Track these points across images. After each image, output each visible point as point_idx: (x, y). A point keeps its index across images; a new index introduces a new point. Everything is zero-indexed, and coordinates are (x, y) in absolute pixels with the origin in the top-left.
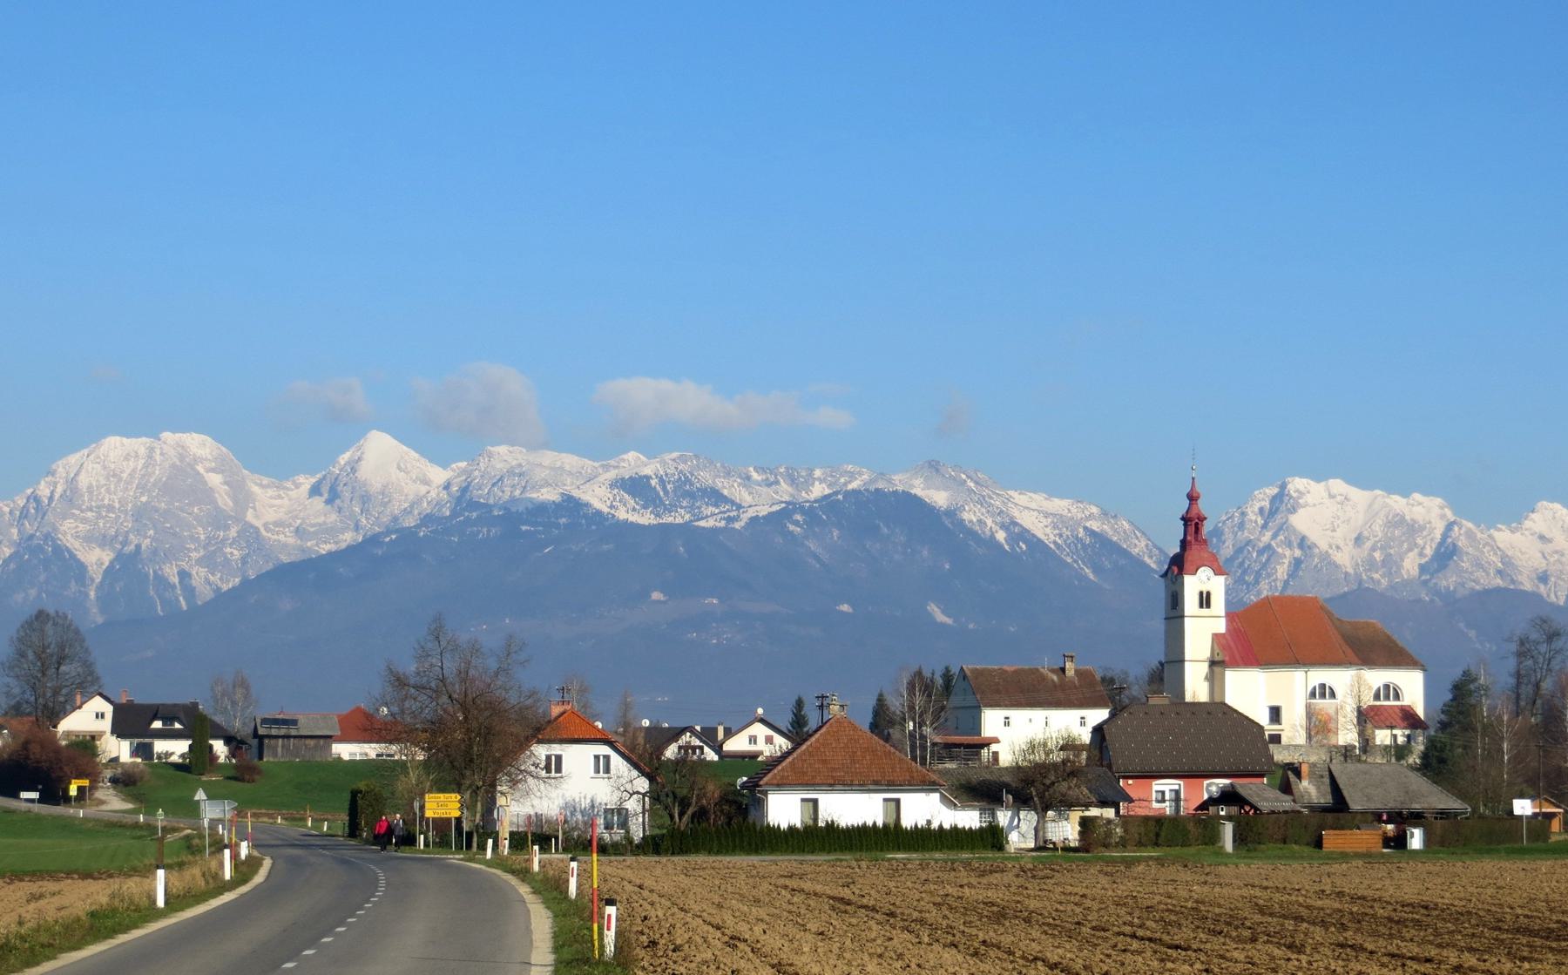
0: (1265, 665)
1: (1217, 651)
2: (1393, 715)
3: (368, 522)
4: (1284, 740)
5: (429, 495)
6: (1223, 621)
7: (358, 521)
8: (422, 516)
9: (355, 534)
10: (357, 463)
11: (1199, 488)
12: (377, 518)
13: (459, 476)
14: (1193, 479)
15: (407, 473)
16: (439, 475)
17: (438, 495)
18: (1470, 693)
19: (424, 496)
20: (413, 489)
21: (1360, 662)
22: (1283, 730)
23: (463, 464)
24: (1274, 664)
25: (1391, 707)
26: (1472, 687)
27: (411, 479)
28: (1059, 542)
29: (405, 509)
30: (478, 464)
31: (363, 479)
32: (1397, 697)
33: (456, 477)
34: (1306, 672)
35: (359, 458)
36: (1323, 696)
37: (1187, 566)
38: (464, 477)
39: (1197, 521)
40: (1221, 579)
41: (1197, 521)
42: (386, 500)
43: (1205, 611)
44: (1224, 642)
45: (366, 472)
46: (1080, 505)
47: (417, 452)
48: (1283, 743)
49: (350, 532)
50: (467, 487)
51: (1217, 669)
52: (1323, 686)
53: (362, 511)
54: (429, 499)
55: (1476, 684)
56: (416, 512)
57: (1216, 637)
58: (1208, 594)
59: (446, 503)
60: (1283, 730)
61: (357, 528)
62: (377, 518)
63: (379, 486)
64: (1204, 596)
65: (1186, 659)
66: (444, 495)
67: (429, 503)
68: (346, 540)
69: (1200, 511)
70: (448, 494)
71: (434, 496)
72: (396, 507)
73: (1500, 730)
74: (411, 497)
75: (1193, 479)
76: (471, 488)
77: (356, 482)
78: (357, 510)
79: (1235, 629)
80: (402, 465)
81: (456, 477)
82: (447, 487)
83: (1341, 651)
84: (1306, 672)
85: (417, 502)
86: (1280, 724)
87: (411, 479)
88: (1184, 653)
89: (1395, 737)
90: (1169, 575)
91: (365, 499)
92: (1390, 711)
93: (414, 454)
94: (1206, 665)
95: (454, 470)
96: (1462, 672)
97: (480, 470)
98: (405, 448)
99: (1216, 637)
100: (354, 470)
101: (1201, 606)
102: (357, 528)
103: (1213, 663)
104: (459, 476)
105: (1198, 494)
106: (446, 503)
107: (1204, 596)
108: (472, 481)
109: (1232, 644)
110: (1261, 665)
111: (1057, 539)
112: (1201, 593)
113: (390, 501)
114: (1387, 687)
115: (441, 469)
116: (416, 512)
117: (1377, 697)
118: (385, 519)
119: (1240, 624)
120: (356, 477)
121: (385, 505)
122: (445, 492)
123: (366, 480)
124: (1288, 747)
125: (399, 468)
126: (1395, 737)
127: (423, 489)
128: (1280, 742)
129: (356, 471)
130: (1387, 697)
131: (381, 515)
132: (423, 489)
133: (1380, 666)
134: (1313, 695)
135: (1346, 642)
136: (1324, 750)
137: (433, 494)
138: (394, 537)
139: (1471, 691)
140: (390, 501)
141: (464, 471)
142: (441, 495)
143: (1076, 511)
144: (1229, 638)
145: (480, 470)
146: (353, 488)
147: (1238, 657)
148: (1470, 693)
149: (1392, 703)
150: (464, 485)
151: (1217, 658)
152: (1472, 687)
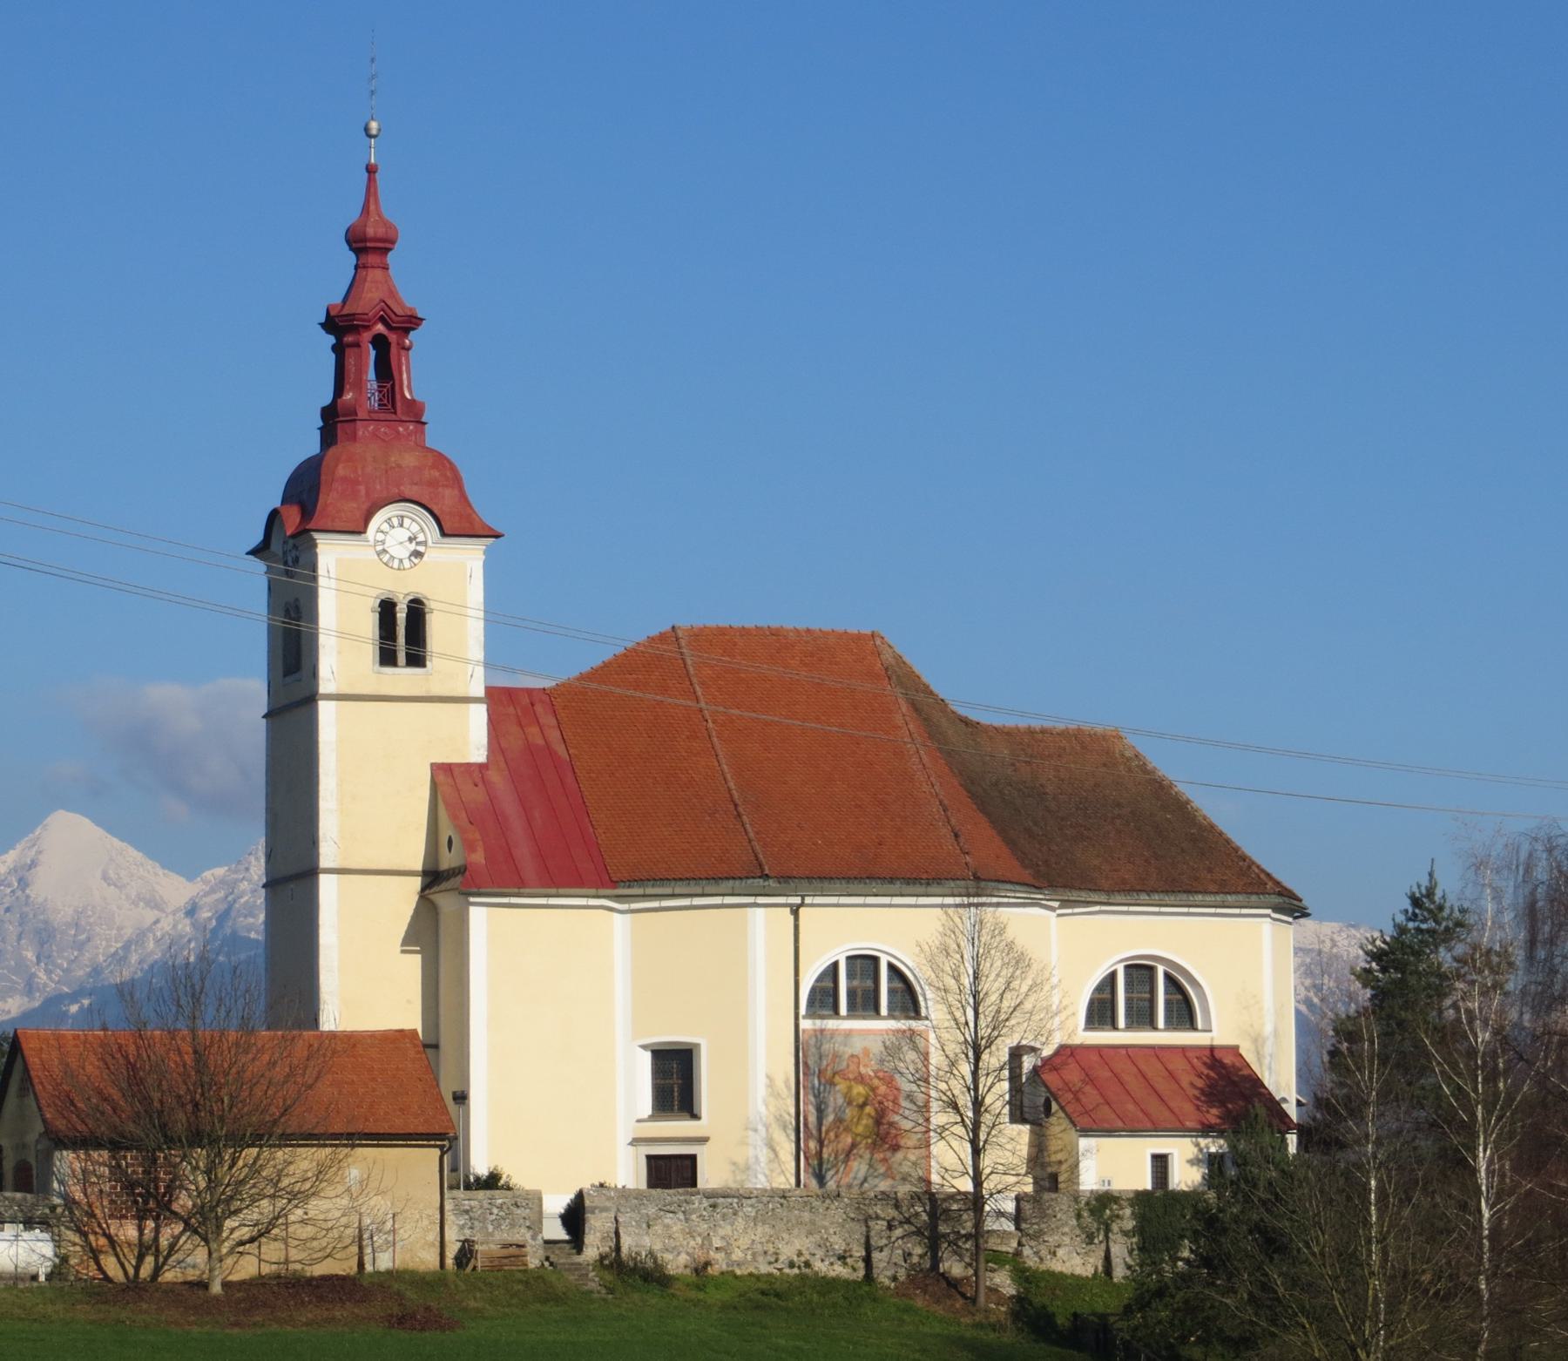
0: (632, 881)
1: (446, 830)
2: (1163, 1086)
3: (51, 979)
4: (710, 1175)
5: (159, 926)
6: (478, 716)
7: (33, 975)
8: (146, 967)
9: (26, 999)
10: (30, 869)
11: (391, 208)
12: (66, 971)
13: (213, 891)
14: (371, 170)
15: (120, 887)
16: (177, 890)
17: (175, 927)
18: (1440, 984)
19: (150, 929)
20: (131, 918)
21: (1026, 874)
22: (703, 1140)
23: (220, 871)
24: (663, 880)
25: (1157, 1052)
26: (1445, 958)
27: (128, 897)
28: (1316, 1000)
29: (116, 953)
30: (247, 869)
31: (40, 900)
32: (1184, 1012)
33: (206, 894)
34: (795, 911)
35: (33, 861)
36: (865, 1003)
37: (329, 499)
38: (221, 894)
39: (380, 328)
40: (470, 557)
41: (380, 328)
42: (83, 937)
43: (402, 678)
44: (476, 796)
45: (44, 888)
46: (1353, 931)
47: (138, 848)
48: (701, 1184)
49: (18, 998)
50: (227, 912)
51: (445, 901)
52: (865, 964)
53: (38, 958)
54: (159, 934)
55: (1460, 949)
56: (134, 958)
57: (444, 775)
58: (417, 611)
59: (189, 941)
60: (703, 1140)
61: (30, 988)
62: (66, 971)
63: (70, 911)
64: (401, 616)
65: (325, 861)
66: (186, 927)
67: (157, 941)
68: (9, 1012)
69: (392, 293)
70: (193, 925)
71: (168, 928)
72: (102, 948)
73: (1459, 1092)
74: (128, 932)
75: (371, 170)
76: (233, 914)
77: (27, 904)
78: (30, 955)
79: (530, 749)
80: (112, 874)
81: (206, 894)
82: (191, 911)
83: (945, 831)
84: (795, 911)
85: (141, 936)
86: (695, 1116)
87: (128, 897)
88: (313, 842)
89: (1161, 1163)
90: (276, 546)
91: (45, 936)
92: (1153, 1070)
93: (134, 854)
94: (417, 883)
95: (205, 882)
96: (1407, 904)
97: (250, 881)
98: (116, 841)
99: (444, 775)
100: (23, 883)
101: (387, 658)
102: (30, 988)
103: (433, 877)
104: (213, 891)
105: (389, 226)
106: (189, 941)
107: (401, 616)
108: (235, 901)
109: (510, 806)
110: (614, 884)
111: (1311, 994)
112: (387, 609)
113: (89, 939)
114: (1140, 972)
115: (182, 879)
116: (134, 958)
117: (1100, 1012)
118: (81, 973)
119: (554, 735)
120: (28, 897)
121: (80, 946)
122: (187, 921)
123: (46, 900)
124: (727, 1200)
125: (105, 878)
126: (1161, 1163)
127: (150, 915)
128: (692, 1181)
129: (27, 885)
130: (1142, 1016)
131: (74, 966)
132: (150, 915)
133: (1109, 892)
134: (823, 998)
135: (982, 805)
136: (837, 1212)
137: (166, 925)
138: (86, 1002)
139: (1443, 977)
140: (89, 939)
141: (222, 882)
142: (180, 927)
143: (1346, 942)
144: (494, 776)
145: (250, 881)
146: (23, 916)
147: (524, 853)
148: (1440, 984)
149: (1162, 1037)
150: (223, 907)
151: (448, 861)
152: (1445, 958)
